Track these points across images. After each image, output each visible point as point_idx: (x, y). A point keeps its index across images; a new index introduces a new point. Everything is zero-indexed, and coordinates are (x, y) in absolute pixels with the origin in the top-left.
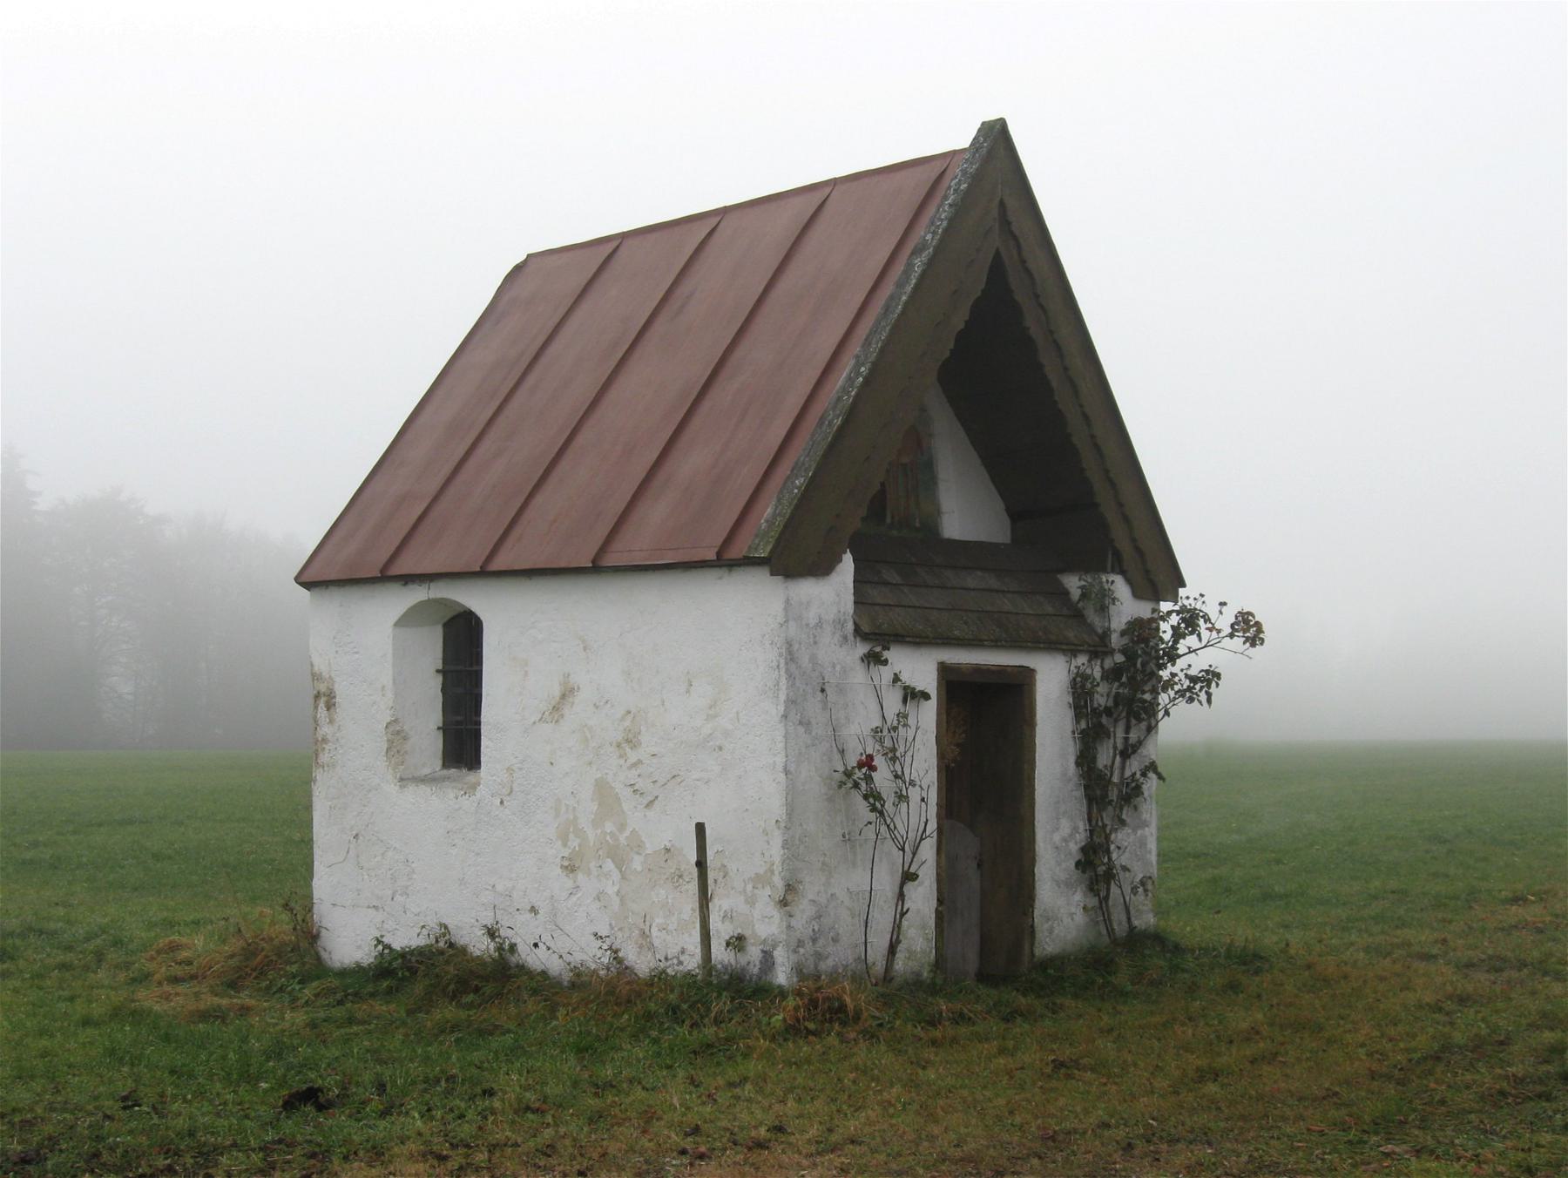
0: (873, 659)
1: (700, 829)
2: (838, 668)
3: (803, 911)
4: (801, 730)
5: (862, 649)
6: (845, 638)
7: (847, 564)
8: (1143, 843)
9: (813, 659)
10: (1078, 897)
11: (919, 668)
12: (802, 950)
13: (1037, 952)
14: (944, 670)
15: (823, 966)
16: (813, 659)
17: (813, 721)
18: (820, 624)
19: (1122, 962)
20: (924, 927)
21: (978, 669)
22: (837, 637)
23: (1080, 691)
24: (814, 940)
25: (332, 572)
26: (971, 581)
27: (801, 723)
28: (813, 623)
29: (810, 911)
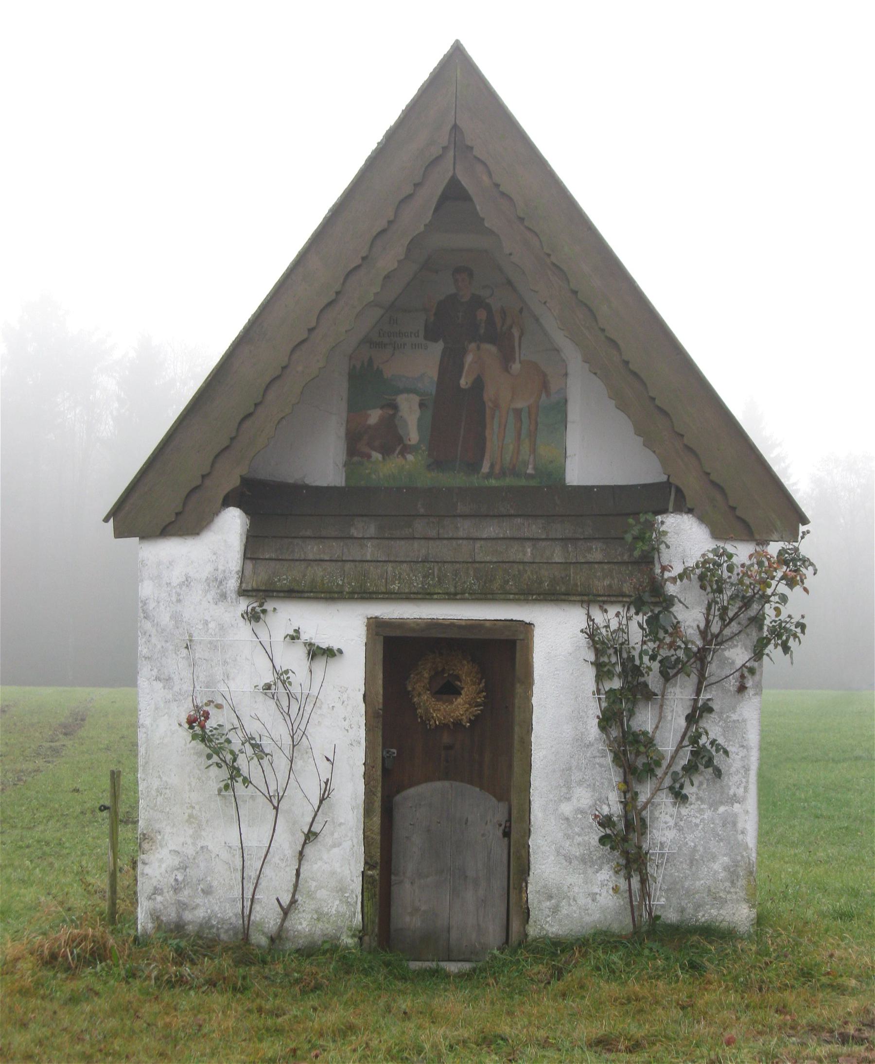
0: (254, 617)
1: (278, 900)
2: (212, 625)
3: (161, 861)
4: (159, 685)
5: (243, 605)
6: (224, 596)
7: (232, 523)
8: (730, 822)
9: (177, 618)
10: (605, 875)
11: (344, 627)
12: (159, 898)
13: (533, 931)
14: (376, 626)
15: (188, 916)
16: (177, 618)
17: (176, 678)
18: (187, 582)
19: (661, 945)
20: (341, 890)
21: (434, 624)
22: (212, 594)
23: (603, 650)
24: (176, 890)
25: (158, 501)
26: (491, 529)
27: (157, 679)
28: (175, 582)
29: (172, 861)
